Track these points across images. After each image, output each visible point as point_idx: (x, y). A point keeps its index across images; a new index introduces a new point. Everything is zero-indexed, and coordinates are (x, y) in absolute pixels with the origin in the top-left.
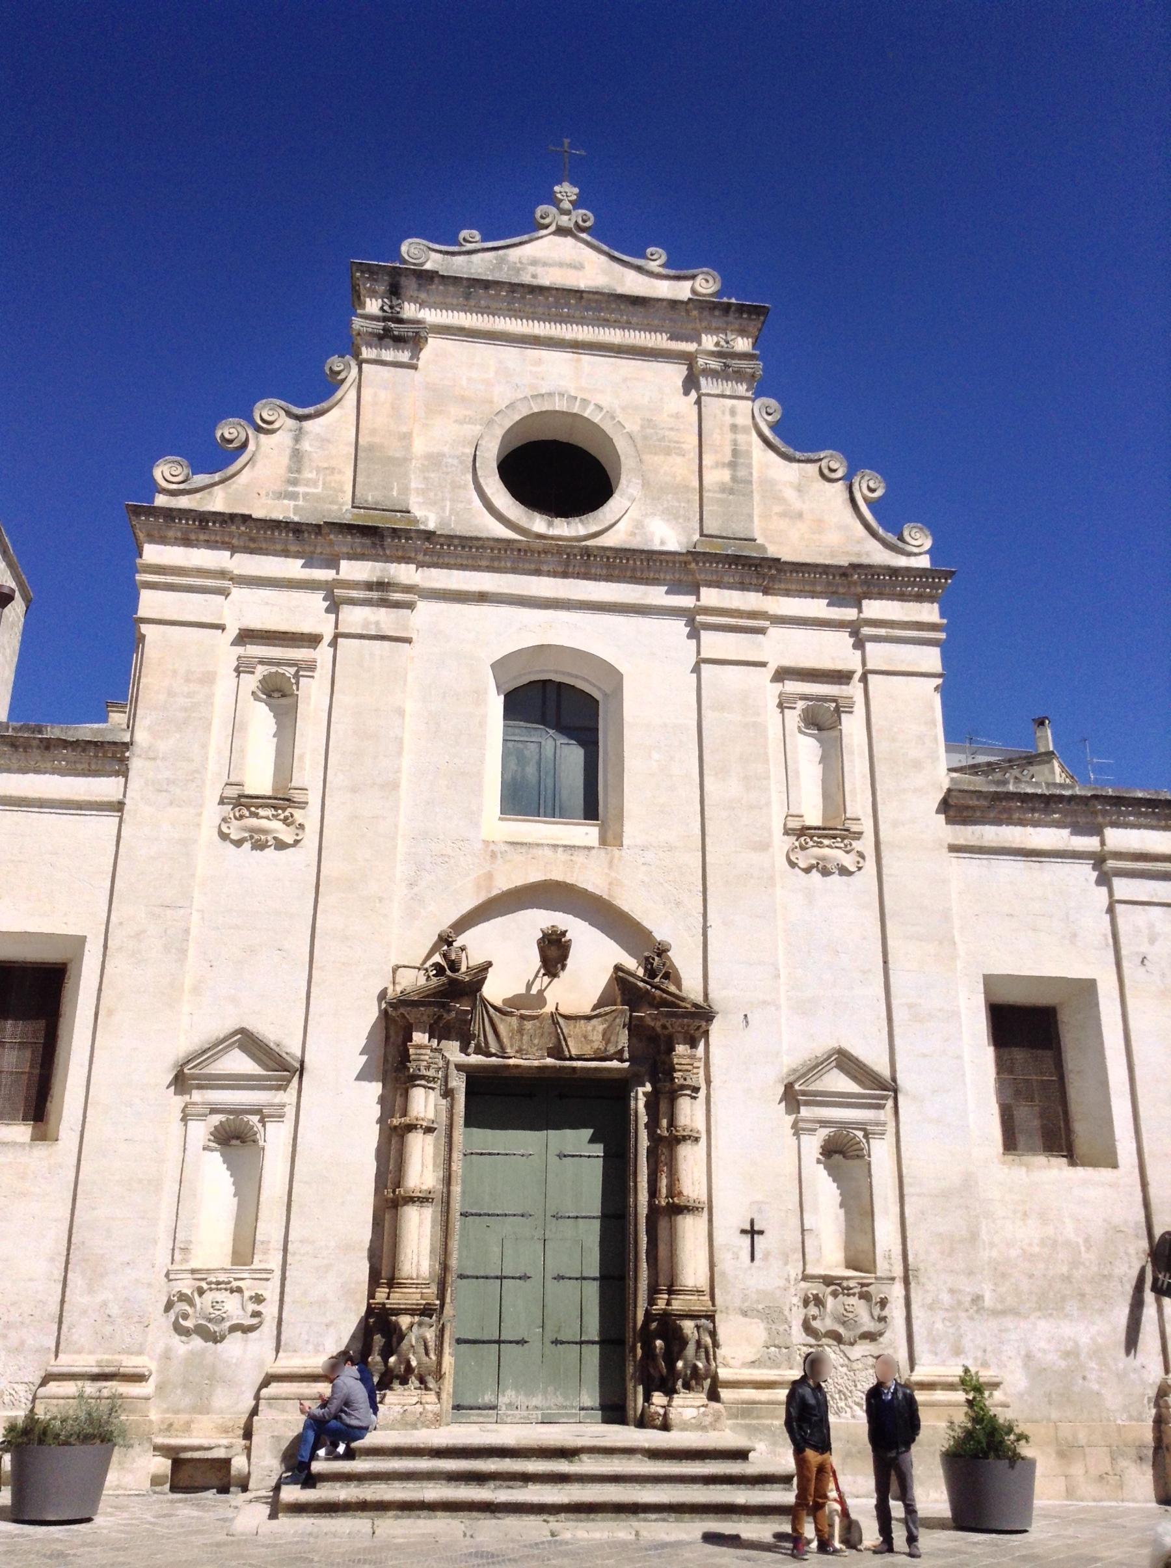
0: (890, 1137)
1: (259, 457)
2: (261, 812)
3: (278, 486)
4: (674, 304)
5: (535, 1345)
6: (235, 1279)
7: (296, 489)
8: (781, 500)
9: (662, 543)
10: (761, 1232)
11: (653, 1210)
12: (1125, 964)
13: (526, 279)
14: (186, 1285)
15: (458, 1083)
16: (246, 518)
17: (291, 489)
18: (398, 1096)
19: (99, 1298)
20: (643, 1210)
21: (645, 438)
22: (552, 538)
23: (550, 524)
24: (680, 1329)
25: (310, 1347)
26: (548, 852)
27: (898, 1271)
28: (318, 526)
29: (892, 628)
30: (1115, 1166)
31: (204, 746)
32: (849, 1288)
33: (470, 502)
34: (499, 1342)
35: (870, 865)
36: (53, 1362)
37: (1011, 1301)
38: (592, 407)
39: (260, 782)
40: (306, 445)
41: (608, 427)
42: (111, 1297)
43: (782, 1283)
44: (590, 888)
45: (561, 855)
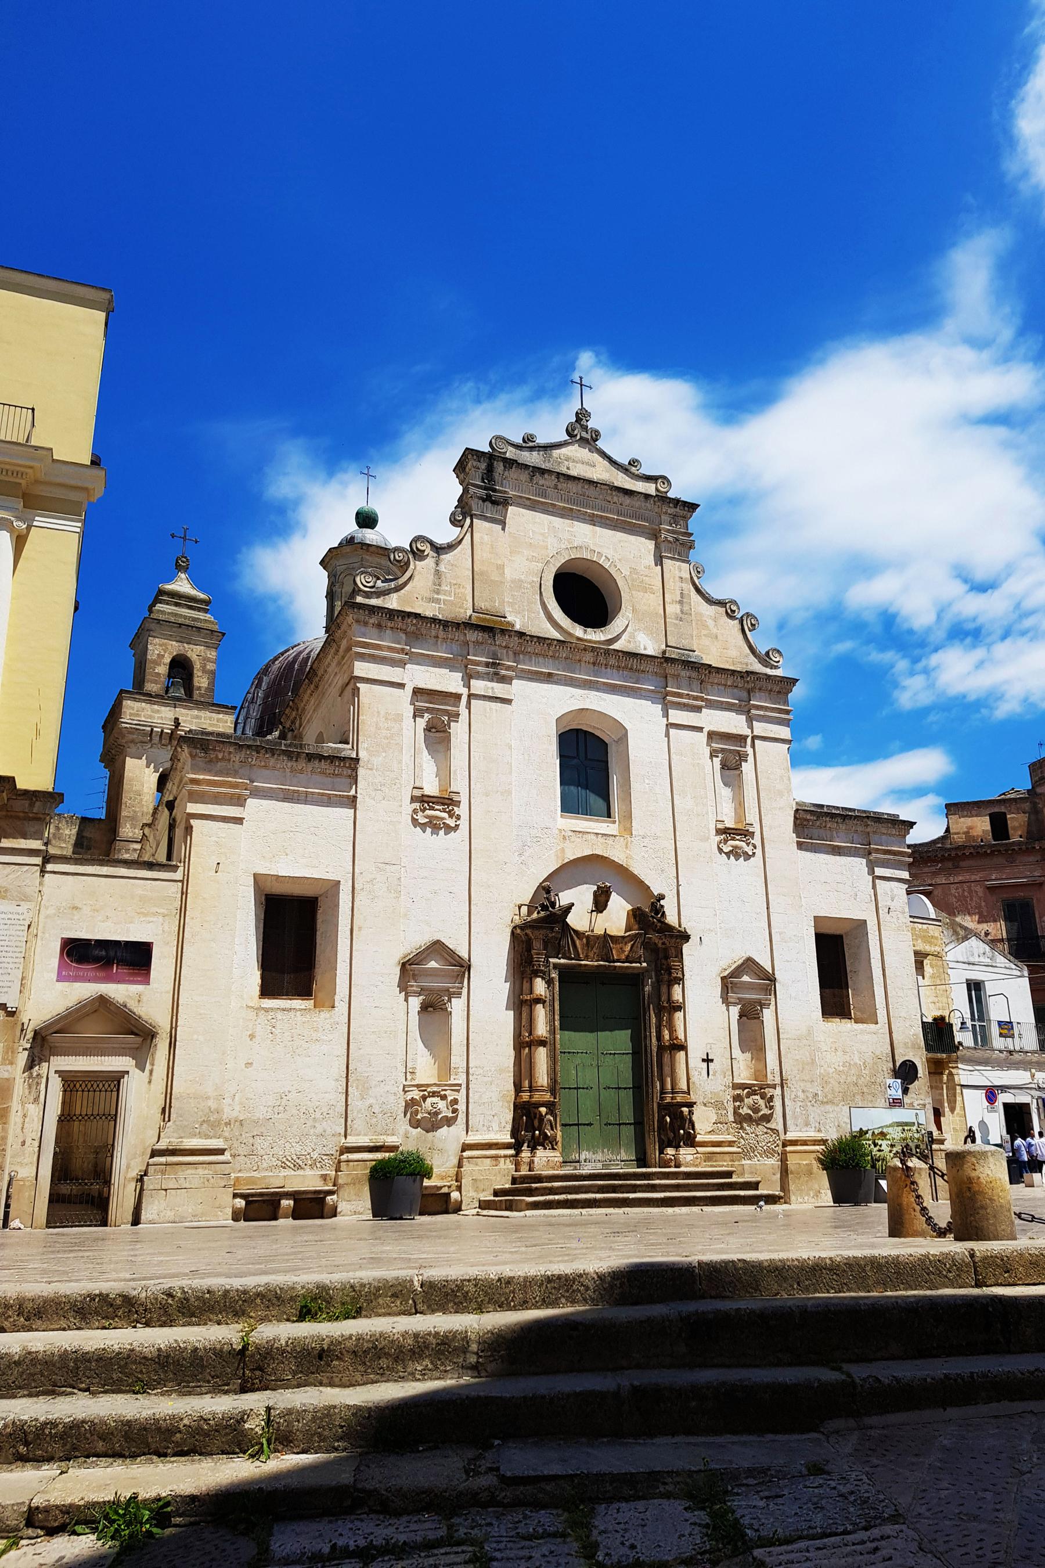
0: (772, 1007)
1: (416, 573)
2: (437, 807)
3: (427, 594)
4: (647, 496)
5: (597, 1126)
6: (443, 1090)
7: (439, 597)
8: (706, 627)
9: (645, 649)
10: (712, 1060)
11: (661, 1048)
12: (880, 911)
13: (563, 470)
14: (416, 1094)
15: (554, 975)
16: (417, 616)
17: (436, 596)
18: (525, 982)
19: (368, 1103)
20: (655, 1049)
21: (633, 580)
22: (586, 640)
23: (585, 632)
24: (682, 1112)
25: (485, 1128)
26: (593, 837)
27: (778, 1081)
28: (458, 624)
29: (766, 711)
30: (877, 1023)
31: (400, 762)
32: (756, 1090)
33: (539, 613)
34: (578, 1125)
35: (759, 851)
36: (343, 1140)
37: (830, 1096)
38: (604, 558)
39: (431, 788)
40: (442, 567)
41: (612, 571)
42: (374, 1102)
43: (723, 1088)
44: (616, 860)
45: (600, 839)
